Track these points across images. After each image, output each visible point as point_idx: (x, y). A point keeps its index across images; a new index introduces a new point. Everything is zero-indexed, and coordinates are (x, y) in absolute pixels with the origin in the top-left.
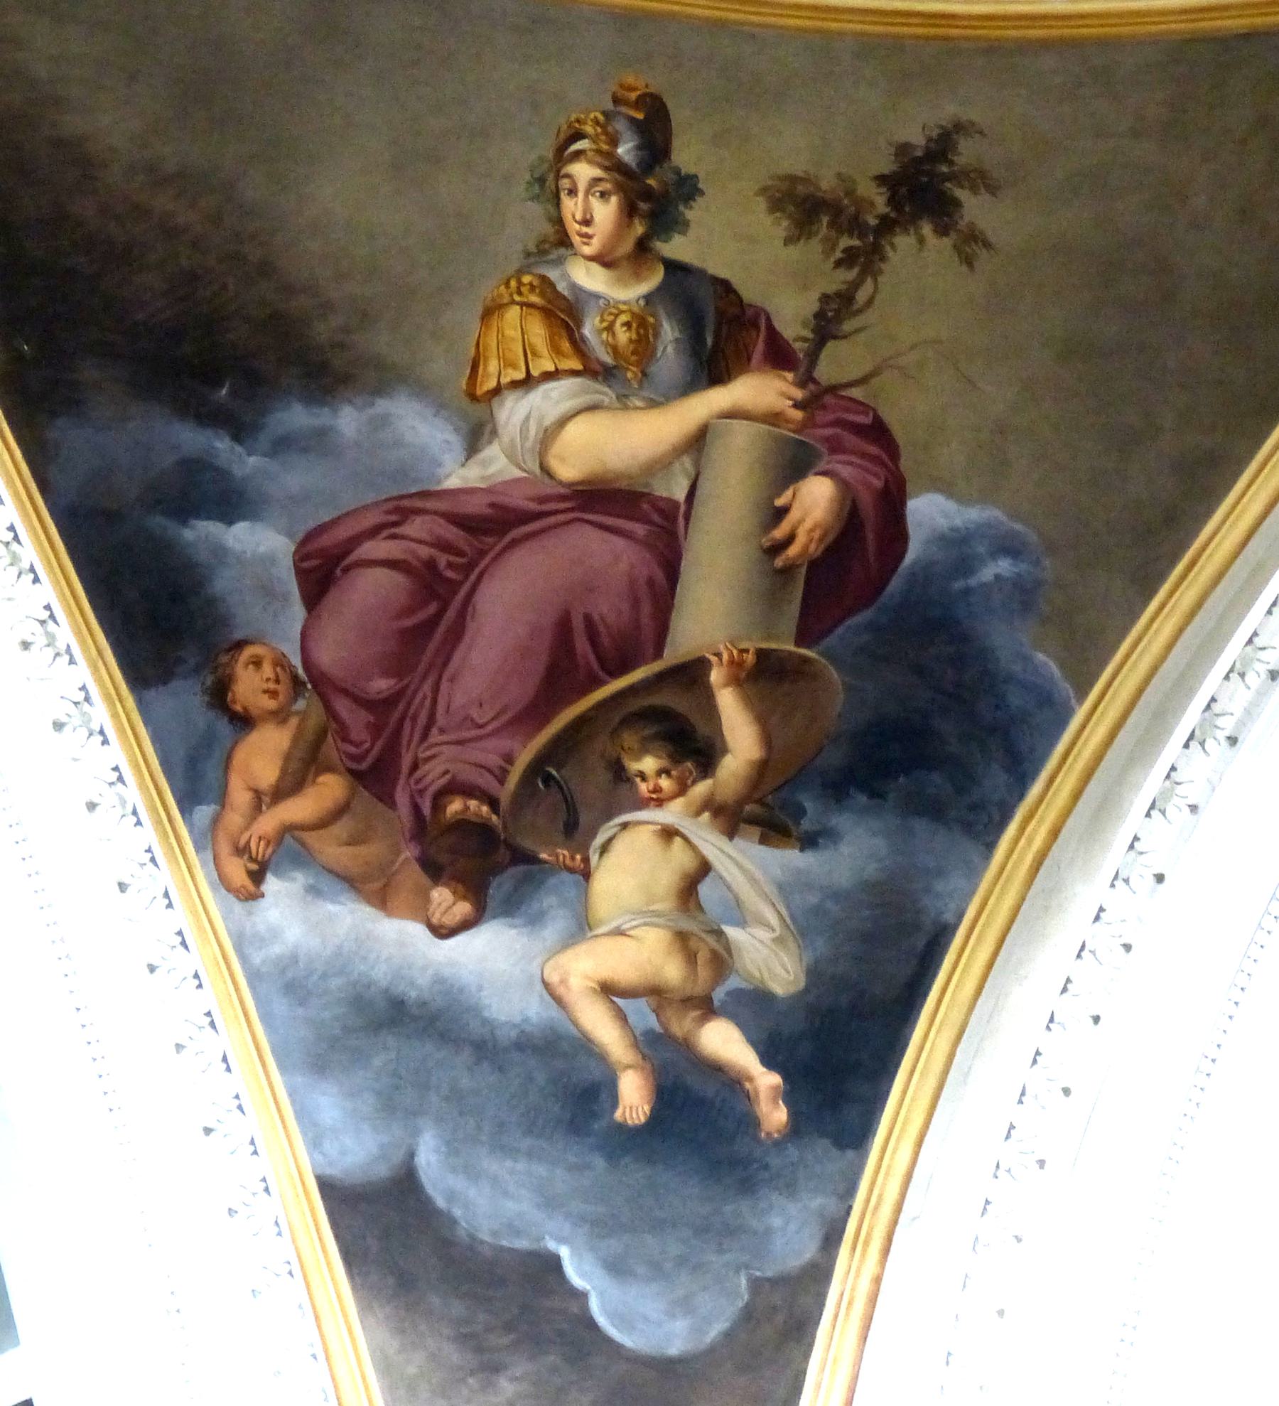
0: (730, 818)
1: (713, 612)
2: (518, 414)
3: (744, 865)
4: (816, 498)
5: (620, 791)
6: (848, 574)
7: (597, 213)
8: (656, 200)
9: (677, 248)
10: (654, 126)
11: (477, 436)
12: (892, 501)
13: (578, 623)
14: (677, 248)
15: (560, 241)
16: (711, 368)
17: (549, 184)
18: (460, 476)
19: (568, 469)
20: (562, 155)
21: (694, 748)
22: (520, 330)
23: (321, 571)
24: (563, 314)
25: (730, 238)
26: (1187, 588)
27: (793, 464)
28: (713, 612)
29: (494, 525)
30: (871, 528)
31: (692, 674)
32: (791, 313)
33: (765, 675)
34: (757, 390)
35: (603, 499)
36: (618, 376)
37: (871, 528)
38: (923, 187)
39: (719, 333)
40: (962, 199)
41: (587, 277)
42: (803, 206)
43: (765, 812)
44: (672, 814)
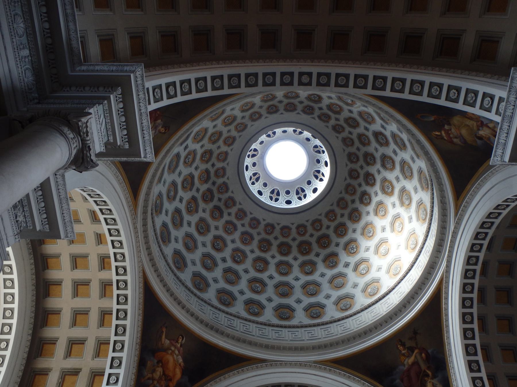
0: (432, 379)
1: (423, 367)
2: (406, 362)
3: (435, 381)
4: (423, 355)
5: (426, 382)
6: (429, 359)
7: (401, 348)
8: (403, 345)
9: (406, 346)
10: (400, 341)
11: (404, 365)
12: (427, 352)
13: (90, 116)
14: (406, 346)
15: (401, 351)
16: (413, 352)
17: (398, 348)
18: (405, 368)
19: (410, 364)
20: (397, 346)
21: (428, 375)
22: (402, 358)
23: (402, 380)
24: (404, 355)
25: (409, 344)
26: (497, 148)
27: (421, 354)
28: (423, 367)
29: (409, 370)
30: (427, 354)
31: (425, 371)
32: (414, 345)
33: (429, 368)
34: (416, 351)
35: (414, 364)
36: (409, 356)
37: (427, 354)
38: (415, 333)
39: (411, 350)
40: (356, 135)
41: (403, 352)
42: (410, 339)
43: (434, 377)
44: (429, 380)
